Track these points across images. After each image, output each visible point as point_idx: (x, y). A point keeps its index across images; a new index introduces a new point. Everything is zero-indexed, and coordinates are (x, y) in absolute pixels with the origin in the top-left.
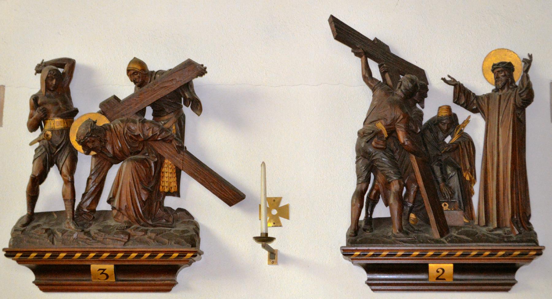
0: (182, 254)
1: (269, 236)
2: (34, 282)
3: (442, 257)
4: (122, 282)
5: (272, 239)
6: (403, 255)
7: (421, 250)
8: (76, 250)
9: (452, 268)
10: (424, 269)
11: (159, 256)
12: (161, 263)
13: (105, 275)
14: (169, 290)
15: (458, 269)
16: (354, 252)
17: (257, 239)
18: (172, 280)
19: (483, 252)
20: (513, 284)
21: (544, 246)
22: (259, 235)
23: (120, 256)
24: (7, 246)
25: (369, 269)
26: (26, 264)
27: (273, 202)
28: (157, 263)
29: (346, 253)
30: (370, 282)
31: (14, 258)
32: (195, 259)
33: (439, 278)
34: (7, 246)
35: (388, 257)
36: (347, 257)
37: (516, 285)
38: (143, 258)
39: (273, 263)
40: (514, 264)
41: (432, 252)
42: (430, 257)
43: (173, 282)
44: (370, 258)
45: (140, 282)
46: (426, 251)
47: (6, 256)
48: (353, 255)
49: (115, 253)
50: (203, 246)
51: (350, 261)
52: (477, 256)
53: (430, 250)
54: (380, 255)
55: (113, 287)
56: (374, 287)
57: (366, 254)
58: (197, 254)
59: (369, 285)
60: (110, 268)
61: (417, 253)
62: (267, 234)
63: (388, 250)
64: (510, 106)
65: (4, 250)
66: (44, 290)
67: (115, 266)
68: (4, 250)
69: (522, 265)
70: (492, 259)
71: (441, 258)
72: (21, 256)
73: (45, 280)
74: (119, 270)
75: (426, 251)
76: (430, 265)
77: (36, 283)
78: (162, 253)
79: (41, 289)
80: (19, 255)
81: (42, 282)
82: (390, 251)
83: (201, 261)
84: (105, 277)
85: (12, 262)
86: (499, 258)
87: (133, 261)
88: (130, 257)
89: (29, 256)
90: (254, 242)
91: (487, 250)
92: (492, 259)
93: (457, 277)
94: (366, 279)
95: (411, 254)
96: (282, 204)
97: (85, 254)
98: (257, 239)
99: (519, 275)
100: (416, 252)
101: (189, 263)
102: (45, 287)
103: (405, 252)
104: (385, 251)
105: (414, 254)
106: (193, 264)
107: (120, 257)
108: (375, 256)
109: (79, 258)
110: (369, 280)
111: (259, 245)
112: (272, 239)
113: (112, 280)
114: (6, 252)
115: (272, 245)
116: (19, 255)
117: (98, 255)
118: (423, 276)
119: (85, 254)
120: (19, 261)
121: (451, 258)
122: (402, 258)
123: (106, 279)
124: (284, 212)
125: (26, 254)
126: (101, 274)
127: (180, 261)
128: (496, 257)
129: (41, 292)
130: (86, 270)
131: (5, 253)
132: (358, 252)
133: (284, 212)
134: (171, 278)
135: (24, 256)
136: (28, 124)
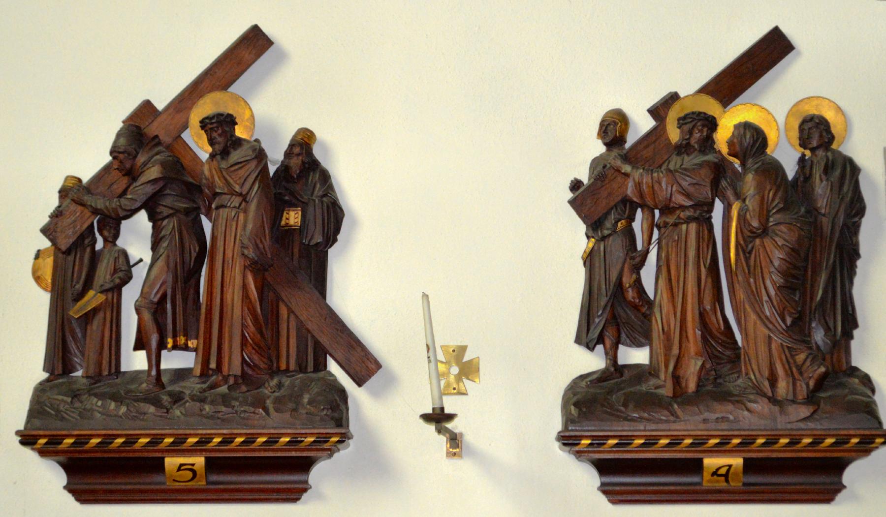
0: (322, 440)
1: (447, 411)
2: (65, 488)
3: (709, 447)
5: (450, 417)
6: (617, 445)
7: (672, 436)
11: (117, 443)
14: (295, 500)
16: (729, 439)
17: (427, 418)
22: (429, 411)
23: (168, 442)
25: (603, 467)
26: (52, 456)
27: (454, 353)
28: (774, 455)
30: (607, 488)
31: (35, 447)
32: (340, 446)
34: (21, 427)
36: (567, 448)
37: (309, 491)
38: (232, 446)
42: (284, 445)
43: (304, 486)
45: (792, 487)
47: (23, 443)
48: (578, 444)
49: (754, 438)
50: (353, 427)
52: (719, 446)
58: (344, 438)
59: (605, 492)
60: (199, 461)
61: (642, 441)
62: (442, 409)
65: (18, 433)
66: (613, 502)
67: (746, 460)
68: (18, 433)
72: (46, 444)
74: (750, 466)
77: (69, 488)
78: (716, 438)
80: (42, 441)
81: (75, 487)
82: (744, 437)
83: (350, 449)
84: (190, 475)
85: (29, 455)
89: (61, 443)
90: (421, 421)
93: (753, 479)
94: (598, 484)
96: (466, 358)
97: (156, 440)
98: (427, 418)
99: (849, 475)
100: (144, 438)
101: (331, 452)
105: (662, 444)
106: (336, 455)
108: (595, 445)
110: (603, 484)
111: (431, 428)
112: (450, 417)
114: (21, 436)
115: (450, 425)
116: (42, 441)
117: (180, 440)
118: (696, 479)
119: (156, 440)
120: (43, 453)
121: (698, 449)
122: (667, 449)
123: (192, 479)
124: (469, 370)
125: (54, 440)
127: (318, 450)
129: (610, 505)
131: (19, 438)
133: (469, 370)
134: (836, 479)
136: (569, 187)
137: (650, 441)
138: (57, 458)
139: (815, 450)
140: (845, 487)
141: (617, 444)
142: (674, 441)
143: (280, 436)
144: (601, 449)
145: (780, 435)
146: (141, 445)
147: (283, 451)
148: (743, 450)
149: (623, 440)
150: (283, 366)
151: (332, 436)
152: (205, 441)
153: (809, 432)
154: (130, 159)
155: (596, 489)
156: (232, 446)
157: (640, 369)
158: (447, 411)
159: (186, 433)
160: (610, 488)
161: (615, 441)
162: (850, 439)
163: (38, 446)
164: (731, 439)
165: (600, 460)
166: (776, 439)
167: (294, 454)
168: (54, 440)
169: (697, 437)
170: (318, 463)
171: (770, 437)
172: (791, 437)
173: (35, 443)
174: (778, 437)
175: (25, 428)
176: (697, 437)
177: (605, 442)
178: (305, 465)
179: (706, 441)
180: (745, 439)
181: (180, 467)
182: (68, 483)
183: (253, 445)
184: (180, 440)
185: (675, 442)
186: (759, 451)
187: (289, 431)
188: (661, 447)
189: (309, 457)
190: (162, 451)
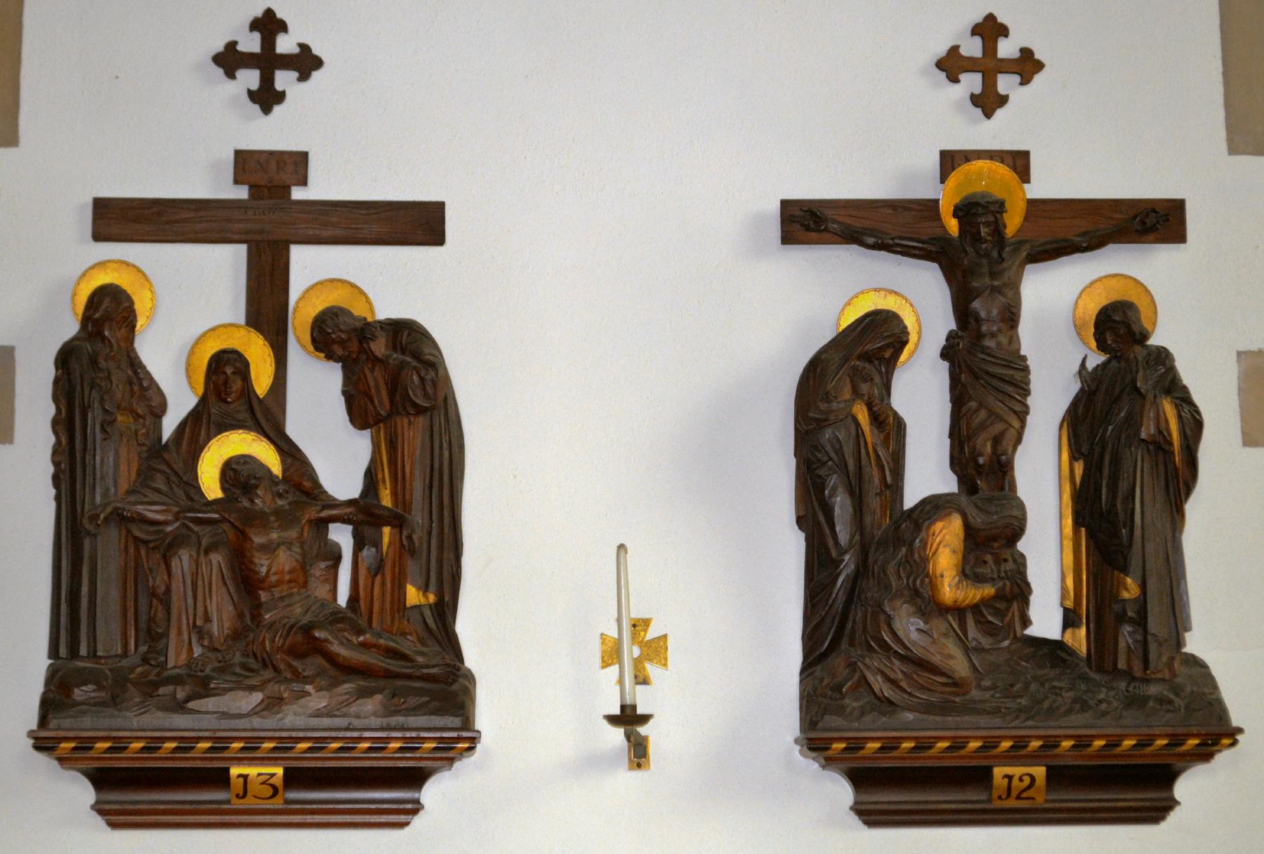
1: (640, 711)
5: (645, 719)
8: (61, 734)
10: (981, 777)
12: (907, 764)
15: (1058, 776)
16: (229, 743)
18: (1165, 799)
20: (415, 812)
25: (860, 778)
28: (929, 763)
29: (43, 744)
30: (863, 807)
33: (1022, 796)
35: (213, 753)
36: (814, 754)
37: (421, 813)
38: (932, 752)
39: (639, 766)
40: (1168, 766)
43: (415, 806)
46: (129, 740)
48: (828, 749)
54: (292, 748)
55: (122, 818)
56: (113, 818)
59: (101, 812)
60: (1040, 772)
64: (202, 571)
66: (114, 825)
67: (286, 770)
70: (920, 758)
73: (116, 797)
86: (393, 755)
87: (971, 758)
90: (605, 722)
91: (138, 739)
92: (920, 758)
95: (160, 748)
99: (1184, 788)
100: (203, 742)
102: (871, 816)
103: (404, 743)
105: (300, 748)
110: (97, 802)
112: (645, 719)
113: (1040, 797)
115: (643, 730)
119: (990, 744)
125: (84, 745)
126: (263, 783)
128: (294, 753)
130: (220, 778)
132: (240, 742)
133: (656, 650)
134: (1164, 795)
138: (840, 766)
139: (1019, 755)
140: (1177, 803)
141: (110, 748)
145: (999, 737)
146: (871, 752)
150: (1122, 665)
152: (1051, 744)
153: (207, 734)
155: (89, 807)
156: (1118, 751)
157: (459, 664)
158: (640, 711)
160: (107, 807)
161: (207, 745)
162: (1123, 740)
163: (58, 753)
164: (831, 744)
165: (99, 770)
166: (1150, 740)
168: (84, 745)
171: (1142, 738)
174: (998, 740)
178: (417, 778)
180: (1141, 740)
181: (240, 776)
182: (856, 803)
184: (1020, 743)
185: (186, 745)
186: (971, 758)
188: (301, 753)
189: (421, 768)
190: (995, 757)
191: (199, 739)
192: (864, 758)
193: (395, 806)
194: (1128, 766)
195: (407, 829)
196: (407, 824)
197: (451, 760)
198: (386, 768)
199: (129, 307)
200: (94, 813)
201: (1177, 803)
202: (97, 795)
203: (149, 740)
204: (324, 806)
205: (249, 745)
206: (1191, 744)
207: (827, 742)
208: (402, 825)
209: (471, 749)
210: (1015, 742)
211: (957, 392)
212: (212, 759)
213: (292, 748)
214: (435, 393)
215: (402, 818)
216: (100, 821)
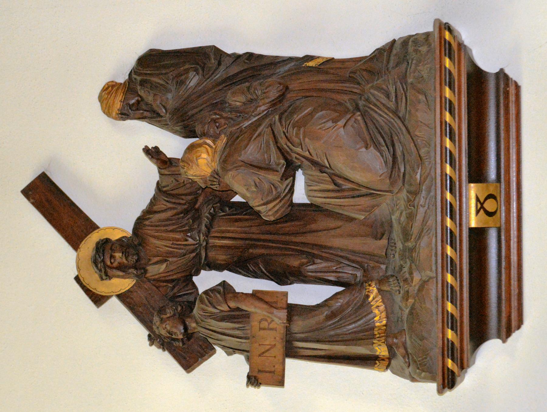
2: (504, 342)
4: (504, 302)
9: (475, 184)
13: (489, 201)
16: (447, 257)
19: (445, 71)
20: (506, 77)
21: (435, 22)
24: (433, 386)
28: (464, 99)
30: (504, 330)
34: (433, 386)
36: (458, 379)
38: (457, 315)
41: (445, 60)
44: (458, 198)
46: (445, 256)
51: (466, 372)
53: (441, 118)
54: (451, 232)
56: (514, 323)
57: (451, 204)
58: (447, 23)
59: (509, 334)
61: (448, 114)
63: (442, 246)
65: (440, 391)
67: (471, 180)
68: (440, 391)
69: (469, 55)
71: (458, 203)
75: (445, 256)
76: (473, 224)
79: (519, 326)
80: (450, 363)
82: (444, 188)
88: (454, 313)
94: (499, 341)
103: (446, 136)
104: (444, 145)
107: (454, 251)
109: (456, 332)
110: (499, 337)
114: (444, 388)
120: (463, 366)
129: (524, 327)
135: (453, 355)
137: (447, 81)
142: (448, 133)
143: (443, 67)
144: (457, 156)
147: (460, 59)
148: (459, 137)
149: (447, 212)
151: (445, 226)
154: (132, 298)
159: (437, 128)
163: (456, 369)
167: (466, 295)
169: (444, 160)
170: (474, 59)
172: (443, 29)
173: (453, 373)
175: (433, 379)
176: (444, 160)
177: (447, 55)
179: (450, 342)
183: (455, 288)
187: (438, 166)
188: (455, 145)
191: (443, 199)
192: (462, 341)
193: (502, 112)
194: (470, 272)
195: (520, 83)
196: (516, 83)
197: (461, 45)
198: (470, 264)
199: (136, 73)
200: (510, 340)
201: (502, 70)
202: (493, 338)
203: (445, 271)
204: (503, 283)
205: (449, 213)
206: (449, 64)
207: (444, 177)
208: (518, 88)
209: (450, 29)
210: (446, 85)
211: (116, 242)
212: (462, 300)
213: (451, 232)
214: (151, 264)
215: (512, 90)
216: (515, 335)
